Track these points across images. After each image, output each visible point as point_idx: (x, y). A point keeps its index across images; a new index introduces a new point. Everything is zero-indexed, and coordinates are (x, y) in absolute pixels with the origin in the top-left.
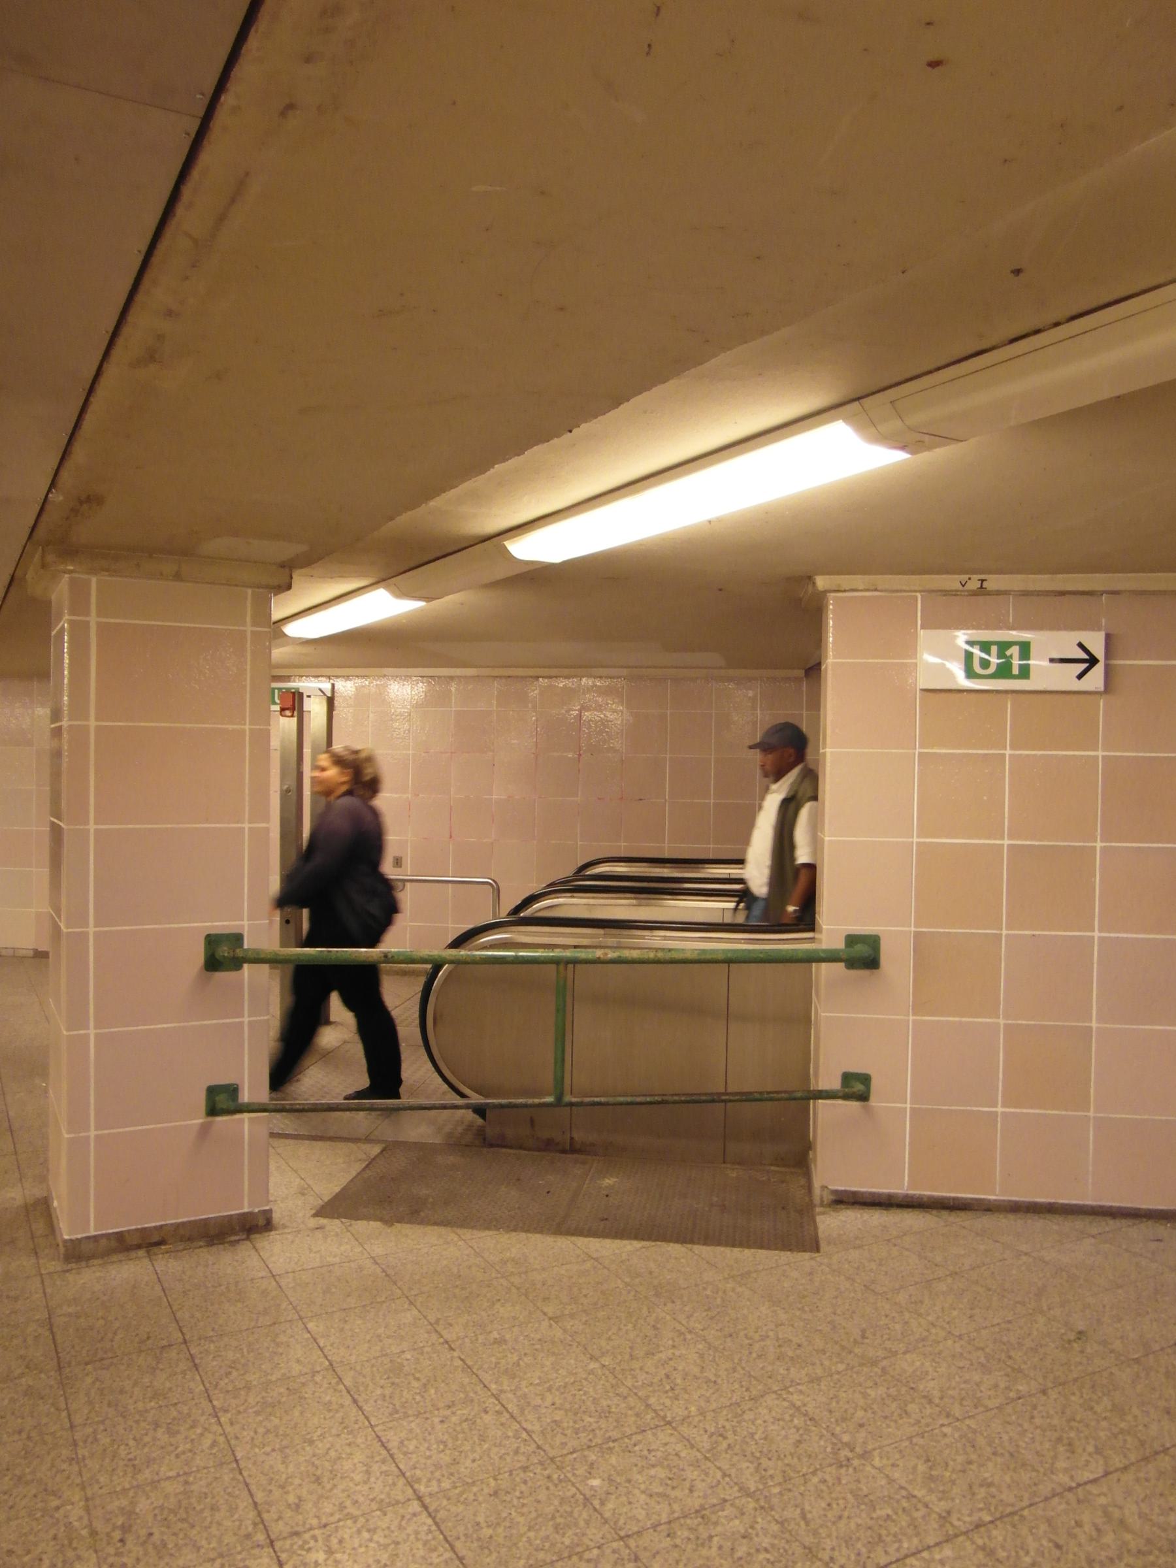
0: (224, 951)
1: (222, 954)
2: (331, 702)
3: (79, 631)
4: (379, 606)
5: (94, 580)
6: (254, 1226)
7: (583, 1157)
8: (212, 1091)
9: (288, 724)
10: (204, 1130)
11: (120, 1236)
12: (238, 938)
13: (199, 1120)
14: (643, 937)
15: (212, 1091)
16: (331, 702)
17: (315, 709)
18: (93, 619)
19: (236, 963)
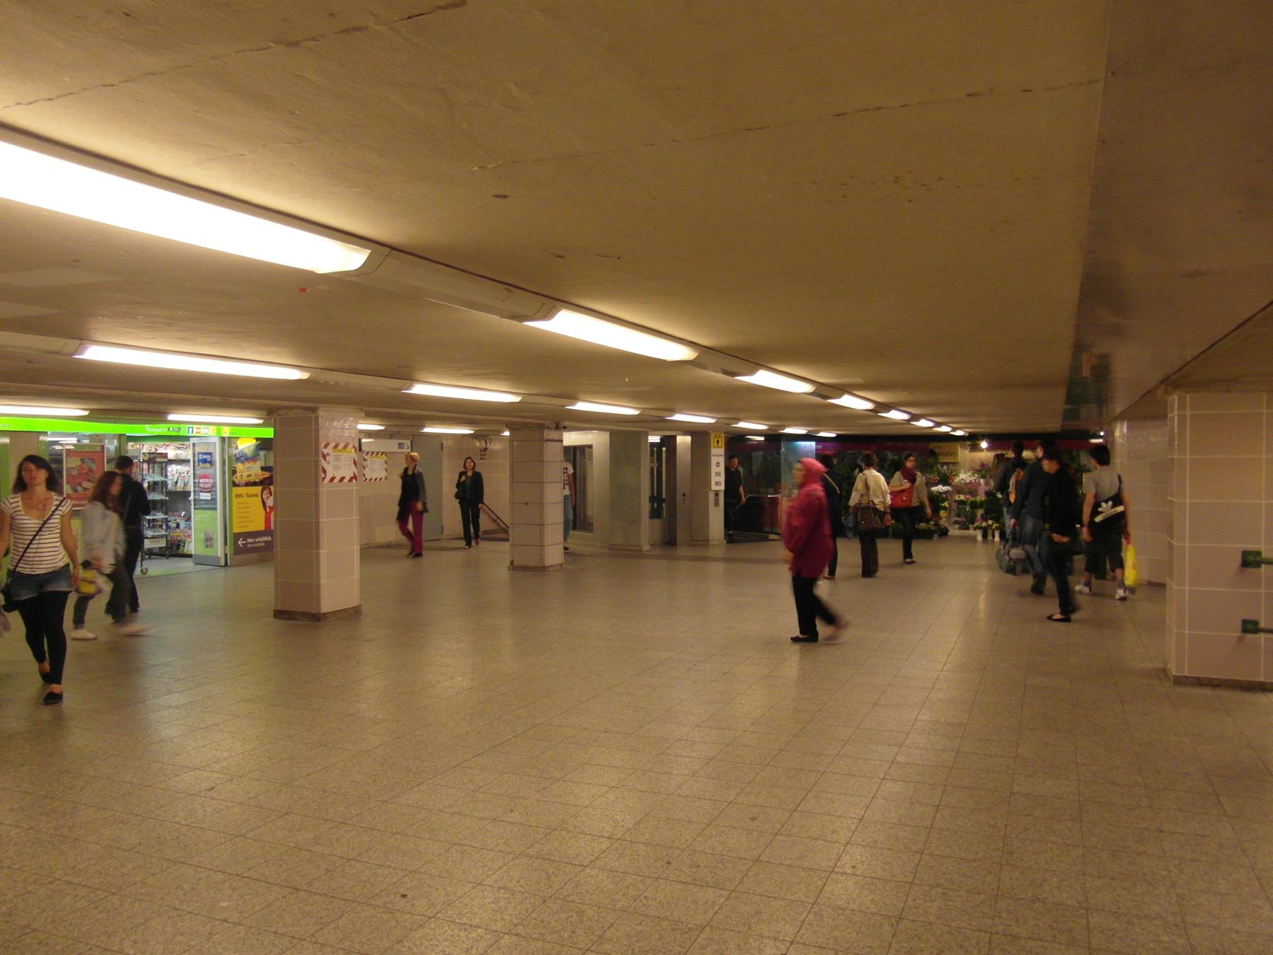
0: (1251, 558)
3: (1182, 419)
8: (1245, 622)
10: (1240, 640)
11: (1199, 679)
15: (1245, 622)
19: (1258, 564)
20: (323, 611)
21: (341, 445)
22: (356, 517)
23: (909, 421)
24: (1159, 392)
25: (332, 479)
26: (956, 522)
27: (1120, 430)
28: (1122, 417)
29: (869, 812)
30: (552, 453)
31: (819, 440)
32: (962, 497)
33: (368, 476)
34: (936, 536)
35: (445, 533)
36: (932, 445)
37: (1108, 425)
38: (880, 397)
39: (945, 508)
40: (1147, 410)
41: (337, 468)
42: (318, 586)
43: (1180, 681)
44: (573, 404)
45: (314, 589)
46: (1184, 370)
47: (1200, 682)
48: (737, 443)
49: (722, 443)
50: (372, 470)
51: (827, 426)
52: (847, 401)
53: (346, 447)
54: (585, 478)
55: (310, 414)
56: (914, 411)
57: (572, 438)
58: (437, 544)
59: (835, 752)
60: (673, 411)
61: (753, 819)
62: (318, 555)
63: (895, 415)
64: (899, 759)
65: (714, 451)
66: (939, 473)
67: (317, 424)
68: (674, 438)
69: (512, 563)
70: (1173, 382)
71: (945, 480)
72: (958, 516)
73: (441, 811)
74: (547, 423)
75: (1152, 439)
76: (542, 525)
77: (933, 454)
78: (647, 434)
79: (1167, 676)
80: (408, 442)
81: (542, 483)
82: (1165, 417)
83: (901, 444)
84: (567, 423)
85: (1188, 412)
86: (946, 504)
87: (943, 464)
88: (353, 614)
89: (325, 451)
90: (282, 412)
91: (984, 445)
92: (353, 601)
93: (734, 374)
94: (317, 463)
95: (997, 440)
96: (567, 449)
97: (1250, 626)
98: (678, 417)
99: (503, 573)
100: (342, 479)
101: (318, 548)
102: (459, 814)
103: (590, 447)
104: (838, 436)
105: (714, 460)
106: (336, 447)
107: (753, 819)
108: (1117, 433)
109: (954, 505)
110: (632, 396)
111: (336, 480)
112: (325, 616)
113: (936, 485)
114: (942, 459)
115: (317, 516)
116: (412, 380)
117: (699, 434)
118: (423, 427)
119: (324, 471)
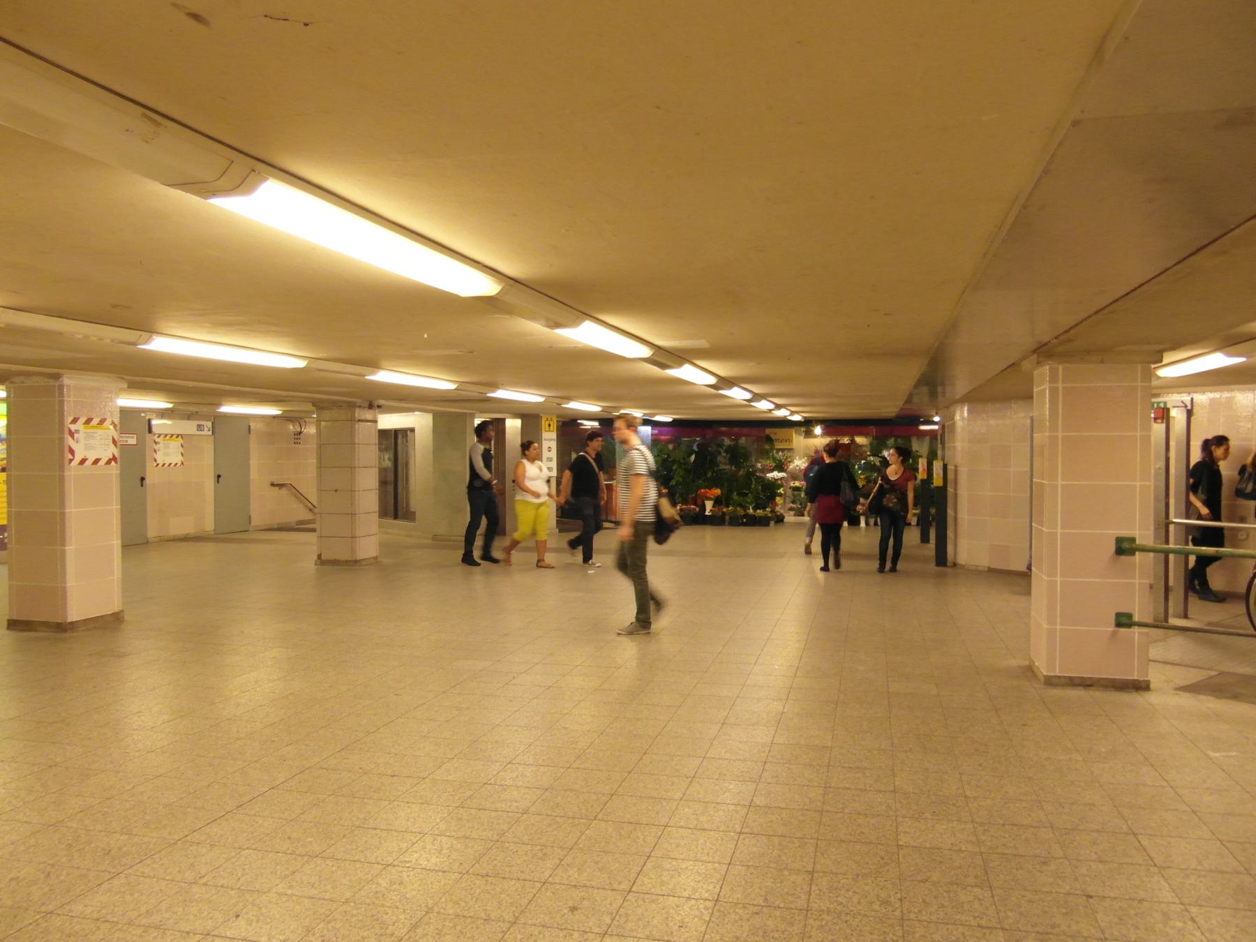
0: (1125, 545)
1: (1124, 548)
2: (1190, 413)
3: (1053, 391)
4: (1217, 360)
5: (1060, 368)
6: (1141, 687)
7: (816, 547)
8: (1118, 615)
9: (1159, 428)
10: (1114, 634)
11: (1070, 678)
12: (1133, 540)
13: (1111, 628)
14: (1210, 624)
15: (1118, 615)
16: (1190, 413)
17: (1178, 415)
18: (1060, 385)
19: (1132, 552)
20: (69, 620)
21: (95, 421)
22: (116, 507)
23: (749, 401)
24: (1026, 365)
25: (83, 461)
26: (791, 509)
27: (962, 415)
28: (962, 401)
29: (726, 890)
30: (365, 437)
31: (655, 424)
32: (797, 484)
33: (160, 461)
34: (772, 523)
35: (255, 522)
36: (768, 431)
37: (947, 408)
38: (723, 369)
39: (780, 495)
40: (1006, 388)
41: (88, 447)
42: (64, 589)
43: (1050, 682)
44: (372, 374)
45: (59, 595)
46: (1072, 332)
47: (1072, 682)
48: (568, 427)
49: (554, 426)
50: (166, 454)
51: (665, 409)
52: (687, 372)
53: (102, 421)
54: (407, 464)
55: (52, 382)
56: (757, 389)
57: (389, 421)
58: (244, 536)
59: (678, 795)
60: (495, 386)
61: (573, 909)
62: (63, 553)
63: (737, 394)
64: (757, 801)
65: (545, 435)
66: (774, 459)
67: (61, 394)
68: (503, 420)
69: (319, 556)
70: (1044, 352)
71: (780, 467)
72: (793, 502)
73: (130, 923)
74: (358, 401)
75: (992, 422)
76: (353, 514)
77: (769, 440)
78: (473, 416)
79: (1034, 675)
80: (209, 424)
81: (352, 468)
82: (1029, 397)
83: (736, 430)
84: (382, 402)
85: (1060, 385)
86: (781, 491)
87: (779, 450)
88: (114, 621)
89: (73, 427)
90: (17, 379)
91: (818, 430)
92: (115, 607)
93: (558, 325)
94: (62, 440)
95: (832, 426)
96: (383, 433)
97: (1124, 620)
98: (501, 394)
99: (309, 565)
100: (96, 461)
101: (63, 544)
102: (157, 928)
103: (412, 430)
104: (675, 421)
105: (545, 445)
106: (89, 421)
107: (573, 909)
108: (957, 417)
109: (789, 492)
110: (446, 364)
111: (88, 463)
112: (73, 626)
113: (772, 471)
114: (778, 446)
115: (62, 504)
116: (150, 330)
117: (530, 418)
118: (220, 405)
119: (72, 452)
